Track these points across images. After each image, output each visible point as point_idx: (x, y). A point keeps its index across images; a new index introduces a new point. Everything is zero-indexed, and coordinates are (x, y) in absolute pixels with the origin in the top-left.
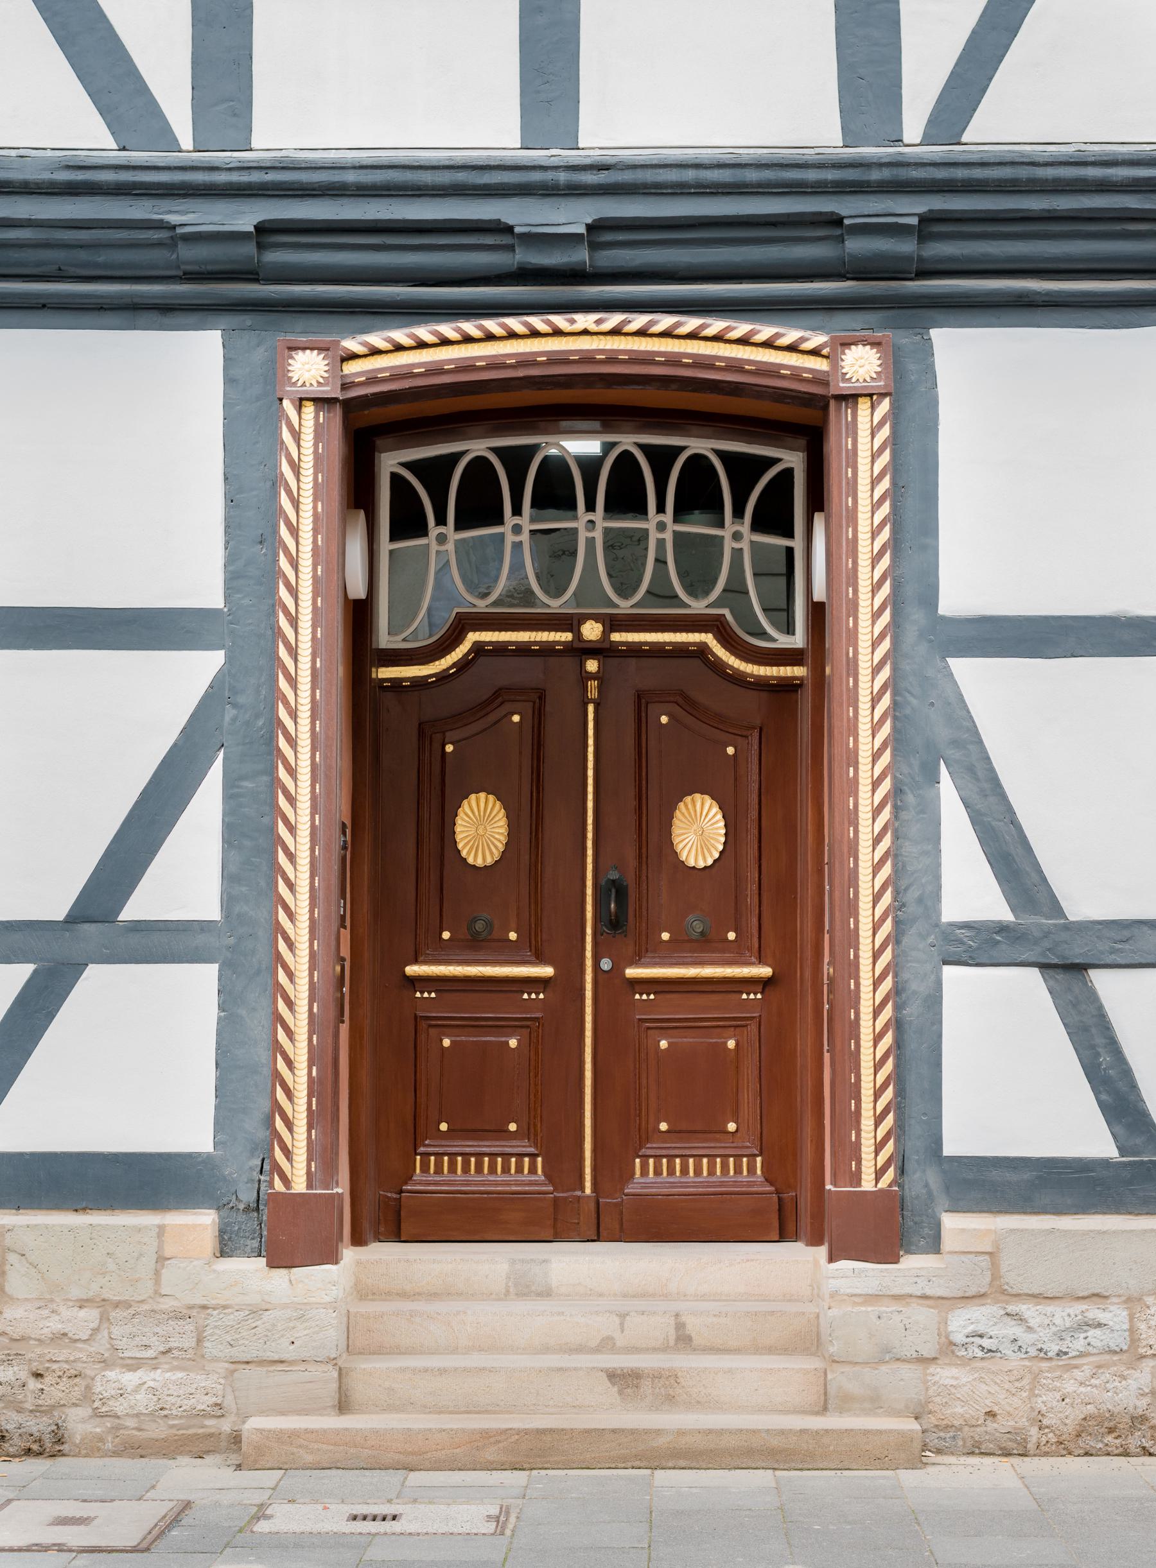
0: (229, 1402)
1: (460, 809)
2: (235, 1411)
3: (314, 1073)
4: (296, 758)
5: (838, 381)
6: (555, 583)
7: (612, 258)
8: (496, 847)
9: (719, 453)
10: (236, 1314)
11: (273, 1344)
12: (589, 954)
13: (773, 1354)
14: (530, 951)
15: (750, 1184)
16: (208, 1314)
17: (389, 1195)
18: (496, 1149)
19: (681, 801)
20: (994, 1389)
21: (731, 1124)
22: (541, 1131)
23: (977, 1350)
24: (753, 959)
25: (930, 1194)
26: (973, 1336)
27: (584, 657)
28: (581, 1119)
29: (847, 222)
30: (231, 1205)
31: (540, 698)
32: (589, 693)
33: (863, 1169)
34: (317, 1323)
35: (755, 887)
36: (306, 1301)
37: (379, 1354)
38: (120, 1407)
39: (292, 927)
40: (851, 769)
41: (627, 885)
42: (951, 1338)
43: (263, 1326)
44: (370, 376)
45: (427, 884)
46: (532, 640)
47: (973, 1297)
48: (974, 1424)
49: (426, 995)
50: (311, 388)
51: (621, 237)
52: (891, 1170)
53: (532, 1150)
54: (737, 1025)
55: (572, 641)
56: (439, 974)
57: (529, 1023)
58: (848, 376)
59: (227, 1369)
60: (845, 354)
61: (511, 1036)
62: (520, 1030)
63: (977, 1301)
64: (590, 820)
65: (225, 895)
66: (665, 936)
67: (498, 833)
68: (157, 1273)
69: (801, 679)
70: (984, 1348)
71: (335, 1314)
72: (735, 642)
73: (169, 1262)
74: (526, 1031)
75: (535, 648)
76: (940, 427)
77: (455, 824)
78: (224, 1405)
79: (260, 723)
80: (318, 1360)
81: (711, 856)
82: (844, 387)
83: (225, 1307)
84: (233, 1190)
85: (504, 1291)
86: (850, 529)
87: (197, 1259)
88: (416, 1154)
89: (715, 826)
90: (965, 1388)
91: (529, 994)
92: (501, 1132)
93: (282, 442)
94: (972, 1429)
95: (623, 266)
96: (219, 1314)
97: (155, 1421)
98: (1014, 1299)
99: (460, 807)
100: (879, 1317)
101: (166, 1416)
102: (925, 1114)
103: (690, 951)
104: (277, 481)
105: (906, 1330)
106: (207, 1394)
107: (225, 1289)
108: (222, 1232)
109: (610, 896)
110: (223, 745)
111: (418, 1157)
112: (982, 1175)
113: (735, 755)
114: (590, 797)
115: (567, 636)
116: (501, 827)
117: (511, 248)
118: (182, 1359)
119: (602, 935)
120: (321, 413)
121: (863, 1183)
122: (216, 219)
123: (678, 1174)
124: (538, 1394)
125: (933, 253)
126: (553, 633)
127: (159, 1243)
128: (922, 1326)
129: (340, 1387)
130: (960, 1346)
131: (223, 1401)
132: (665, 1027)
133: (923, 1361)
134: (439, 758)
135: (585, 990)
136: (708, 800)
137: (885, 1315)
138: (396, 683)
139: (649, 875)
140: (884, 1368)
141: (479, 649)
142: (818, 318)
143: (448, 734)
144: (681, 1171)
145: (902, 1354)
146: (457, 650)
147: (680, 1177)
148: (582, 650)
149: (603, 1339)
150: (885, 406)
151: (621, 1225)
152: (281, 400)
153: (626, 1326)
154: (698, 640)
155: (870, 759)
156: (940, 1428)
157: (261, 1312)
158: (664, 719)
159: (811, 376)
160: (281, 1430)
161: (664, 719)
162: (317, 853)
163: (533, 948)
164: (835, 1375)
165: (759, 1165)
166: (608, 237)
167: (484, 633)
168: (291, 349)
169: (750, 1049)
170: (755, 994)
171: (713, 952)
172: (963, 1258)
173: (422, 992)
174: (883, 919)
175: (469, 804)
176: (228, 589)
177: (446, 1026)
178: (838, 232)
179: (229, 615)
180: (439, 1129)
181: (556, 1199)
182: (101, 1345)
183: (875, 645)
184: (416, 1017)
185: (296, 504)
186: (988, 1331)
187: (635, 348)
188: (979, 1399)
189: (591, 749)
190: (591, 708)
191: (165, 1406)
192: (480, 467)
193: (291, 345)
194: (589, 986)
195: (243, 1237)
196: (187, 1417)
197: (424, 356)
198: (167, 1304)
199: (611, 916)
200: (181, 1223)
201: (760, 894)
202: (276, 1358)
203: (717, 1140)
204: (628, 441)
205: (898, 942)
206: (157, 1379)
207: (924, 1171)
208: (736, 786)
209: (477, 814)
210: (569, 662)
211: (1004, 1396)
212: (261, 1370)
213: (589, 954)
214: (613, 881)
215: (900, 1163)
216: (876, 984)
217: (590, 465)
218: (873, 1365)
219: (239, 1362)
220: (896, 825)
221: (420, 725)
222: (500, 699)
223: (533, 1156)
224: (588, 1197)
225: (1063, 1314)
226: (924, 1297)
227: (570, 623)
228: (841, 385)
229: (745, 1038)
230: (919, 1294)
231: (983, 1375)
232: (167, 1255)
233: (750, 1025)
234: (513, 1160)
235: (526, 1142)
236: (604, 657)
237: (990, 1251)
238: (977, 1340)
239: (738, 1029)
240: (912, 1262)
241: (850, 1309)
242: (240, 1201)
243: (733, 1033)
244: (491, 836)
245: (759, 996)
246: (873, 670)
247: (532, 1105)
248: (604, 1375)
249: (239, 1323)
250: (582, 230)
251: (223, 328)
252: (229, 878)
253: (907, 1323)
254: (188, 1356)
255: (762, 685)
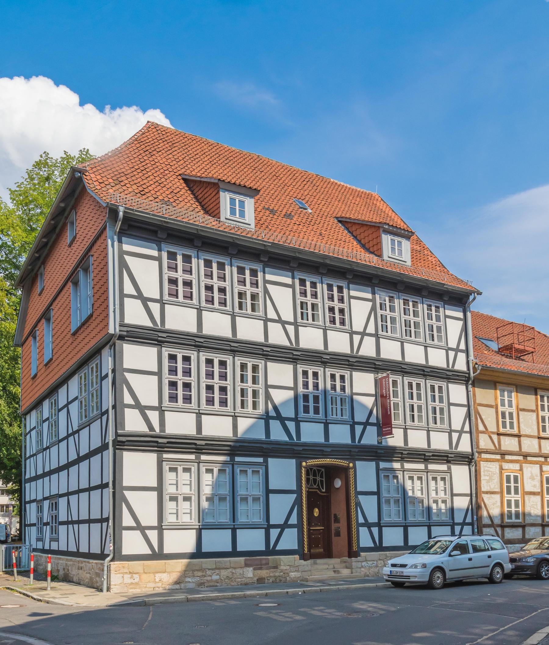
7: (332, 453)
38: (292, 577)
54: (320, 534)
133: (360, 568)
182: (290, 570)
225: (371, 562)
240: (359, 558)
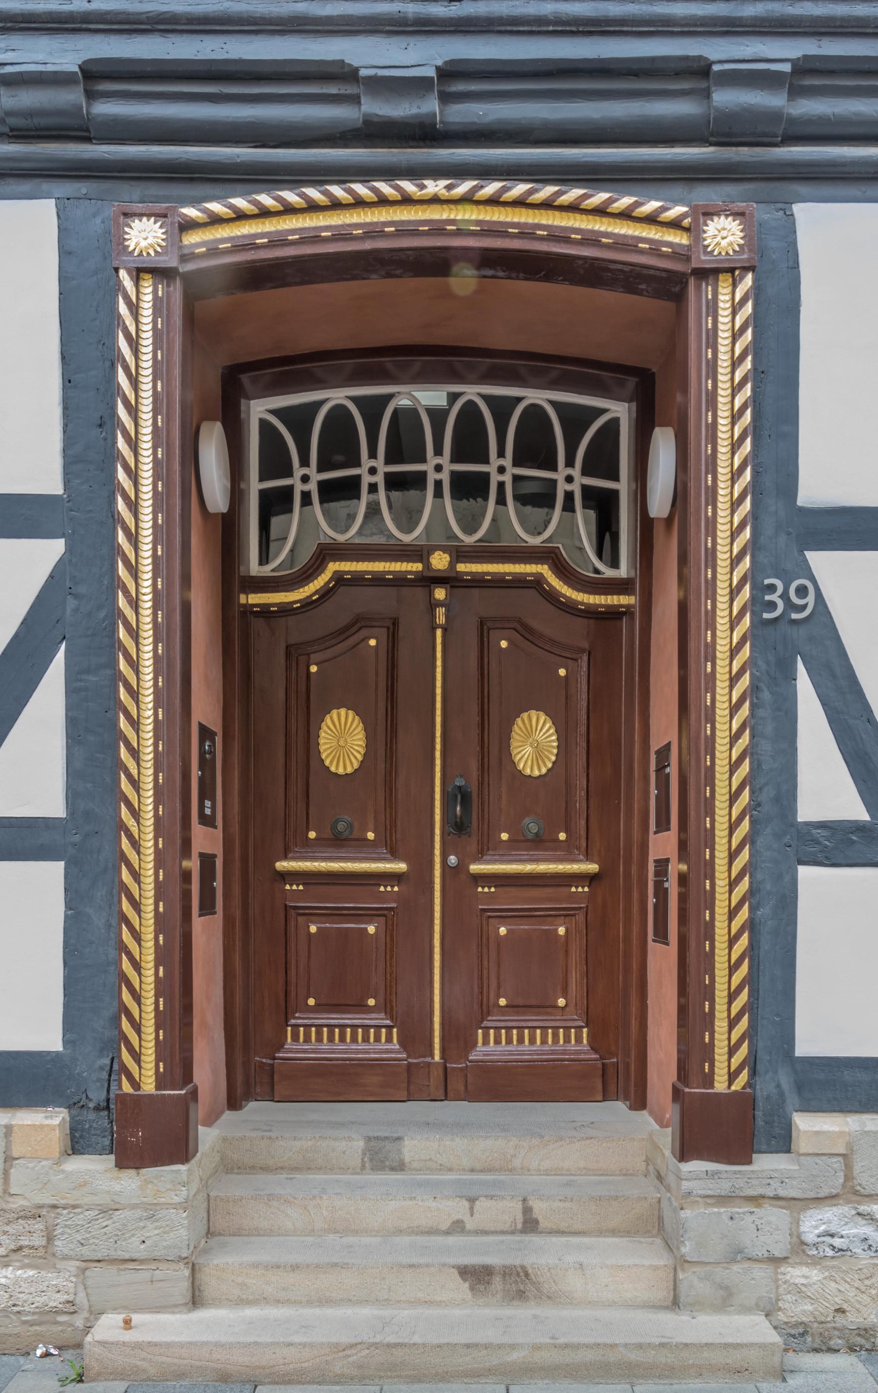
0: (81, 1298)
1: (323, 724)
2: (86, 1307)
3: (161, 974)
4: (138, 650)
5: (699, 253)
6: (408, 520)
8: (355, 757)
9: (552, 403)
10: (87, 1213)
11: (123, 1243)
12: (437, 852)
13: (616, 1237)
14: (386, 849)
15: (577, 1052)
16: (58, 1214)
17: (264, 1061)
18: (357, 1021)
19: (519, 717)
20: (844, 1287)
21: (561, 1000)
22: (396, 1006)
23: (827, 1249)
24: (581, 857)
25: (781, 1094)
26: (824, 1236)
27: (433, 586)
28: (431, 1002)
29: (716, 68)
30: (82, 1103)
31: (394, 624)
32: (437, 619)
33: (716, 1070)
34: (168, 1223)
35: (583, 793)
36: (155, 1201)
37: (239, 1235)
39: (135, 824)
40: (709, 664)
41: (471, 792)
42: (803, 1238)
43: (114, 1225)
44: (211, 247)
45: (295, 788)
46: (387, 569)
47: (826, 1198)
48: (823, 1320)
49: (295, 887)
50: (149, 258)
51: (474, 87)
52: (745, 1072)
53: (388, 1022)
54: (566, 914)
55: (422, 571)
56: (305, 869)
57: (385, 912)
58: (709, 249)
59: (78, 1267)
60: (707, 225)
61: (370, 923)
62: (377, 918)
63: (829, 1202)
64: (438, 733)
65: (70, 792)
66: (504, 836)
67: (358, 745)
68: (6, 1173)
69: (628, 607)
70: (834, 1247)
71: (185, 1215)
72: (569, 573)
73: (17, 1162)
74: (383, 919)
75: (389, 577)
76: (802, 309)
77: (319, 737)
78: (77, 1302)
79: (102, 614)
80: (170, 1259)
81: (545, 765)
82: (702, 261)
83: (74, 1207)
84: (83, 1089)
85: (360, 1165)
86: (710, 414)
87: (46, 1159)
88: (288, 1026)
89: (548, 739)
90: (815, 1286)
91: (385, 887)
92: (361, 1007)
93: (119, 316)
94: (821, 1326)
95: (475, 123)
96: (69, 1213)
97: (8, 1316)
98: (866, 1199)
99: (323, 721)
100: (731, 1218)
101: (19, 1312)
102: (778, 1015)
103: (526, 850)
104: (114, 359)
105: (758, 1230)
106: (59, 1292)
107: (74, 1189)
108: (73, 1130)
109: (456, 800)
110: (64, 638)
111: (289, 1028)
112: (834, 1075)
113: (566, 677)
114: (438, 712)
115: (418, 567)
116: (359, 739)
117: (355, 100)
118: (33, 1257)
119: (449, 835)
120: (160, 286)
121: (716, 1084)
122: (41, 57)
123: (515, 1042)
124: (389, 1290)
125: (804, 110)
126: (405, 564)
127: (6, 1143)
128: (774, 1227)
129: (193, 1283)
130: (812, 1246)
131: (75, 1299)
132: (505, 916)
134: (304, 678)
135: (434, 883)
136: (543, 717)
137: (737, 1216)
138: (265, 612)
139: (490, 782)
140: (736, 1268)
141: (339, 579)
142: (678, 190)
143: (312, 656)
144: (518, 1041)
145: (754, 1254)
146: (319, 578)
147: (517, 1045)
148: (430, 580)
149: (454, 1223)
150: (749, 280)
151: (466, 1086)
152: (117, 270)
153: (475, 1211)
154: (534, 571)
155: (728, 654)
156: (789, 1325)
157: (111, 1212)
158: (504, 644)
159: (670, 250)
160: (123, 1342)
161: (504, 644)
162: (160, 748)
163: (388, 847)
164: (686, 1275)
165: (585, 1035)
166: (460, 87)
167: (343, 563)
168: (126, 215)
169: (578, 935)
170: (583, 887)
171: (546, 850)
172: (817, 1159)
173: (291, 885)
174: (740, 818)
175: (331, 718)
176: (67, 474)
177: (311, 914)
178: (703, 85)
179: (68, 502)
180: (307, 1004)
181: (410, 1065)
183: (734, 535)
184: (286, 905)
185: (135, 383)
186: (839, 1230)
187: (488, 218)
188: (829, 1297)
189: (439, 670)
190: (439, 633)
191: (17, 1303)
192: (340, 415)
193: (126, 211)
194: (437, 880)
195: (94, 1135)
196: (40, 1313)
197: (267, 226)
198: (16, 1204)
199: (456, 818)
200: (29, 1123)
201: (587, 800)
202: (127, 1256)
203: (548, 1014)
204: (472, 392)
205: (753, 843)
206: (10, 1276)
207: (776, 1072)
208: (567, 703)
209: (338, 727)
210: (419, 593)
211: (853, 1294)
212: (113, 1269)
213: (437, 852)
214: (460, 787)
215: (752, 1065)
216: (732, 885)
217: (438, 416)
218: (725, 1265)
219: (90, 1261)
220: (752, 723)
221: (287, 647)
222: (359, 625)
223: (389, 1028)
224: (437, 1063)
226: (777, 1198)
227: (419, 553)
228: (703, 258)
229: (574, 925)
230: (772, 1195)
231: (833, 1274)
232: (15, 1155)
233: (578, 914)
234: (372, 1030)
235: (382, 1015)
236: (452, 587)
237: (844, 1152)
238: (828, 1239)
239: (567, 918)
241: (702, 1210)
242: (91, 1100)
243: (562, 922)
244: (351, 747)
245: (586, 889)
246: (732, 561)
247: (388, 984)
248: (455, 1271)
249: (90, 1223)
250: (431, 73)
251: (57, 196)
252: (73, 774)
253: (759, 1224)
254: (38, 1254)
255: (592, 613)
